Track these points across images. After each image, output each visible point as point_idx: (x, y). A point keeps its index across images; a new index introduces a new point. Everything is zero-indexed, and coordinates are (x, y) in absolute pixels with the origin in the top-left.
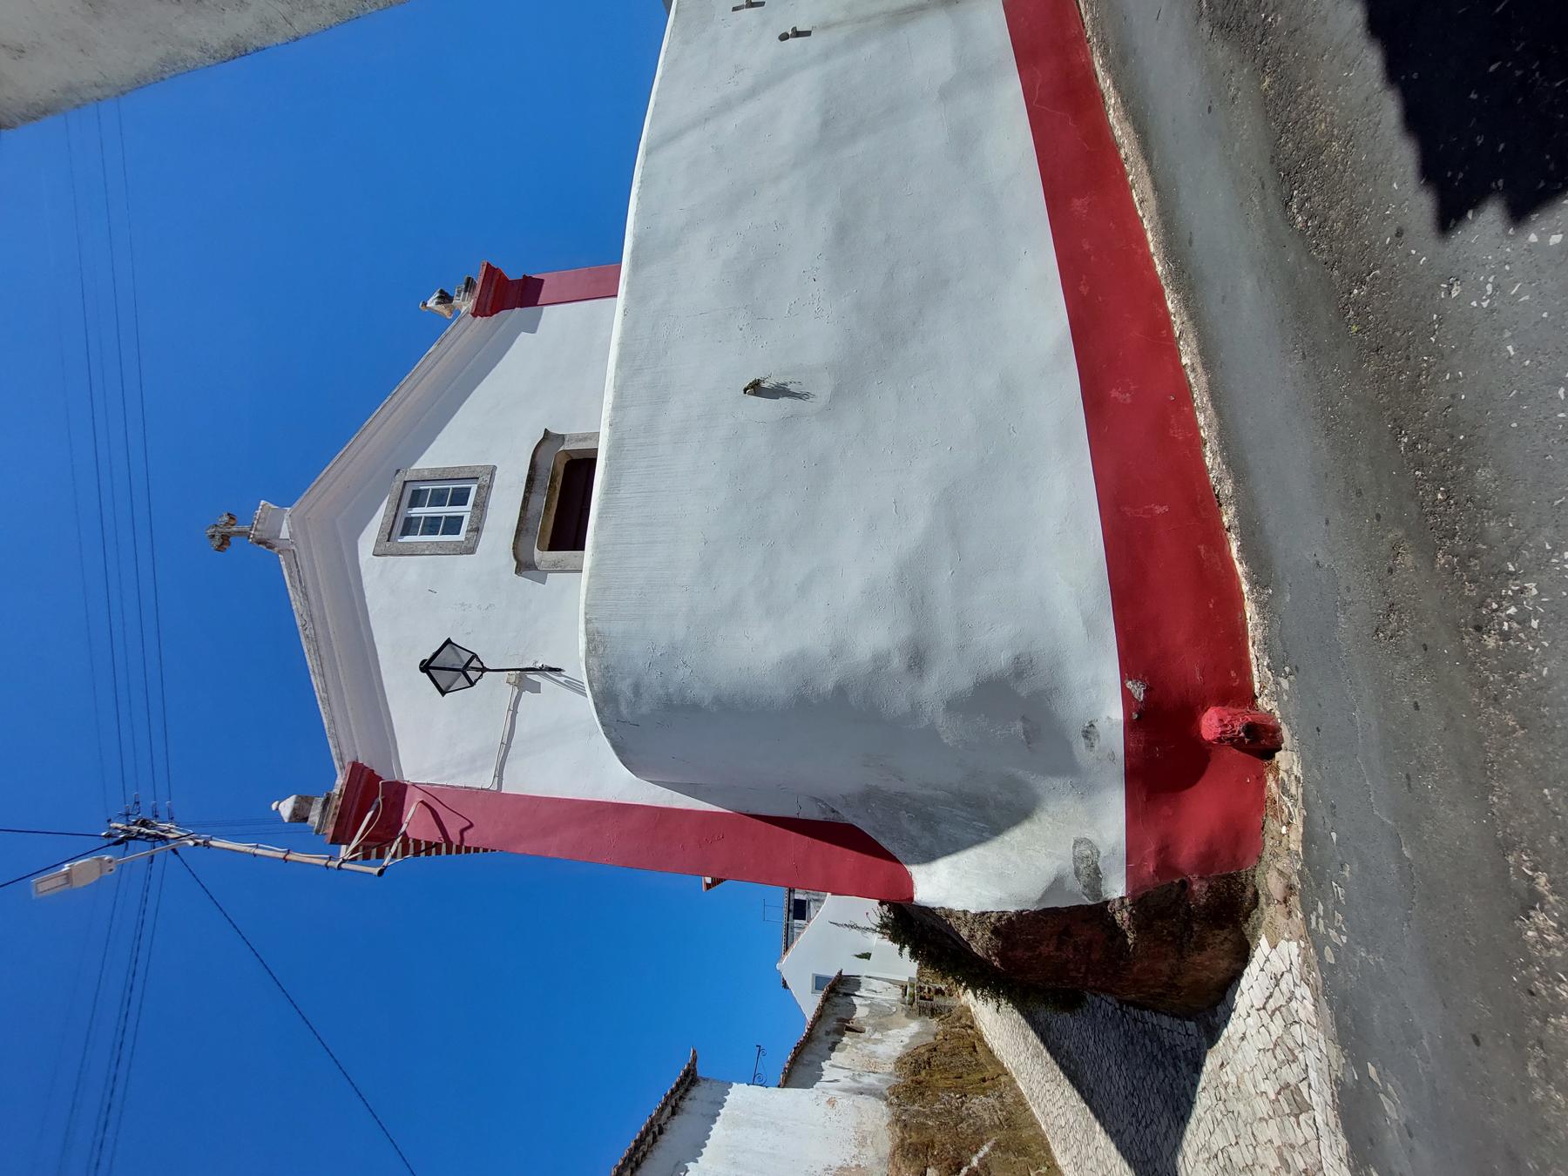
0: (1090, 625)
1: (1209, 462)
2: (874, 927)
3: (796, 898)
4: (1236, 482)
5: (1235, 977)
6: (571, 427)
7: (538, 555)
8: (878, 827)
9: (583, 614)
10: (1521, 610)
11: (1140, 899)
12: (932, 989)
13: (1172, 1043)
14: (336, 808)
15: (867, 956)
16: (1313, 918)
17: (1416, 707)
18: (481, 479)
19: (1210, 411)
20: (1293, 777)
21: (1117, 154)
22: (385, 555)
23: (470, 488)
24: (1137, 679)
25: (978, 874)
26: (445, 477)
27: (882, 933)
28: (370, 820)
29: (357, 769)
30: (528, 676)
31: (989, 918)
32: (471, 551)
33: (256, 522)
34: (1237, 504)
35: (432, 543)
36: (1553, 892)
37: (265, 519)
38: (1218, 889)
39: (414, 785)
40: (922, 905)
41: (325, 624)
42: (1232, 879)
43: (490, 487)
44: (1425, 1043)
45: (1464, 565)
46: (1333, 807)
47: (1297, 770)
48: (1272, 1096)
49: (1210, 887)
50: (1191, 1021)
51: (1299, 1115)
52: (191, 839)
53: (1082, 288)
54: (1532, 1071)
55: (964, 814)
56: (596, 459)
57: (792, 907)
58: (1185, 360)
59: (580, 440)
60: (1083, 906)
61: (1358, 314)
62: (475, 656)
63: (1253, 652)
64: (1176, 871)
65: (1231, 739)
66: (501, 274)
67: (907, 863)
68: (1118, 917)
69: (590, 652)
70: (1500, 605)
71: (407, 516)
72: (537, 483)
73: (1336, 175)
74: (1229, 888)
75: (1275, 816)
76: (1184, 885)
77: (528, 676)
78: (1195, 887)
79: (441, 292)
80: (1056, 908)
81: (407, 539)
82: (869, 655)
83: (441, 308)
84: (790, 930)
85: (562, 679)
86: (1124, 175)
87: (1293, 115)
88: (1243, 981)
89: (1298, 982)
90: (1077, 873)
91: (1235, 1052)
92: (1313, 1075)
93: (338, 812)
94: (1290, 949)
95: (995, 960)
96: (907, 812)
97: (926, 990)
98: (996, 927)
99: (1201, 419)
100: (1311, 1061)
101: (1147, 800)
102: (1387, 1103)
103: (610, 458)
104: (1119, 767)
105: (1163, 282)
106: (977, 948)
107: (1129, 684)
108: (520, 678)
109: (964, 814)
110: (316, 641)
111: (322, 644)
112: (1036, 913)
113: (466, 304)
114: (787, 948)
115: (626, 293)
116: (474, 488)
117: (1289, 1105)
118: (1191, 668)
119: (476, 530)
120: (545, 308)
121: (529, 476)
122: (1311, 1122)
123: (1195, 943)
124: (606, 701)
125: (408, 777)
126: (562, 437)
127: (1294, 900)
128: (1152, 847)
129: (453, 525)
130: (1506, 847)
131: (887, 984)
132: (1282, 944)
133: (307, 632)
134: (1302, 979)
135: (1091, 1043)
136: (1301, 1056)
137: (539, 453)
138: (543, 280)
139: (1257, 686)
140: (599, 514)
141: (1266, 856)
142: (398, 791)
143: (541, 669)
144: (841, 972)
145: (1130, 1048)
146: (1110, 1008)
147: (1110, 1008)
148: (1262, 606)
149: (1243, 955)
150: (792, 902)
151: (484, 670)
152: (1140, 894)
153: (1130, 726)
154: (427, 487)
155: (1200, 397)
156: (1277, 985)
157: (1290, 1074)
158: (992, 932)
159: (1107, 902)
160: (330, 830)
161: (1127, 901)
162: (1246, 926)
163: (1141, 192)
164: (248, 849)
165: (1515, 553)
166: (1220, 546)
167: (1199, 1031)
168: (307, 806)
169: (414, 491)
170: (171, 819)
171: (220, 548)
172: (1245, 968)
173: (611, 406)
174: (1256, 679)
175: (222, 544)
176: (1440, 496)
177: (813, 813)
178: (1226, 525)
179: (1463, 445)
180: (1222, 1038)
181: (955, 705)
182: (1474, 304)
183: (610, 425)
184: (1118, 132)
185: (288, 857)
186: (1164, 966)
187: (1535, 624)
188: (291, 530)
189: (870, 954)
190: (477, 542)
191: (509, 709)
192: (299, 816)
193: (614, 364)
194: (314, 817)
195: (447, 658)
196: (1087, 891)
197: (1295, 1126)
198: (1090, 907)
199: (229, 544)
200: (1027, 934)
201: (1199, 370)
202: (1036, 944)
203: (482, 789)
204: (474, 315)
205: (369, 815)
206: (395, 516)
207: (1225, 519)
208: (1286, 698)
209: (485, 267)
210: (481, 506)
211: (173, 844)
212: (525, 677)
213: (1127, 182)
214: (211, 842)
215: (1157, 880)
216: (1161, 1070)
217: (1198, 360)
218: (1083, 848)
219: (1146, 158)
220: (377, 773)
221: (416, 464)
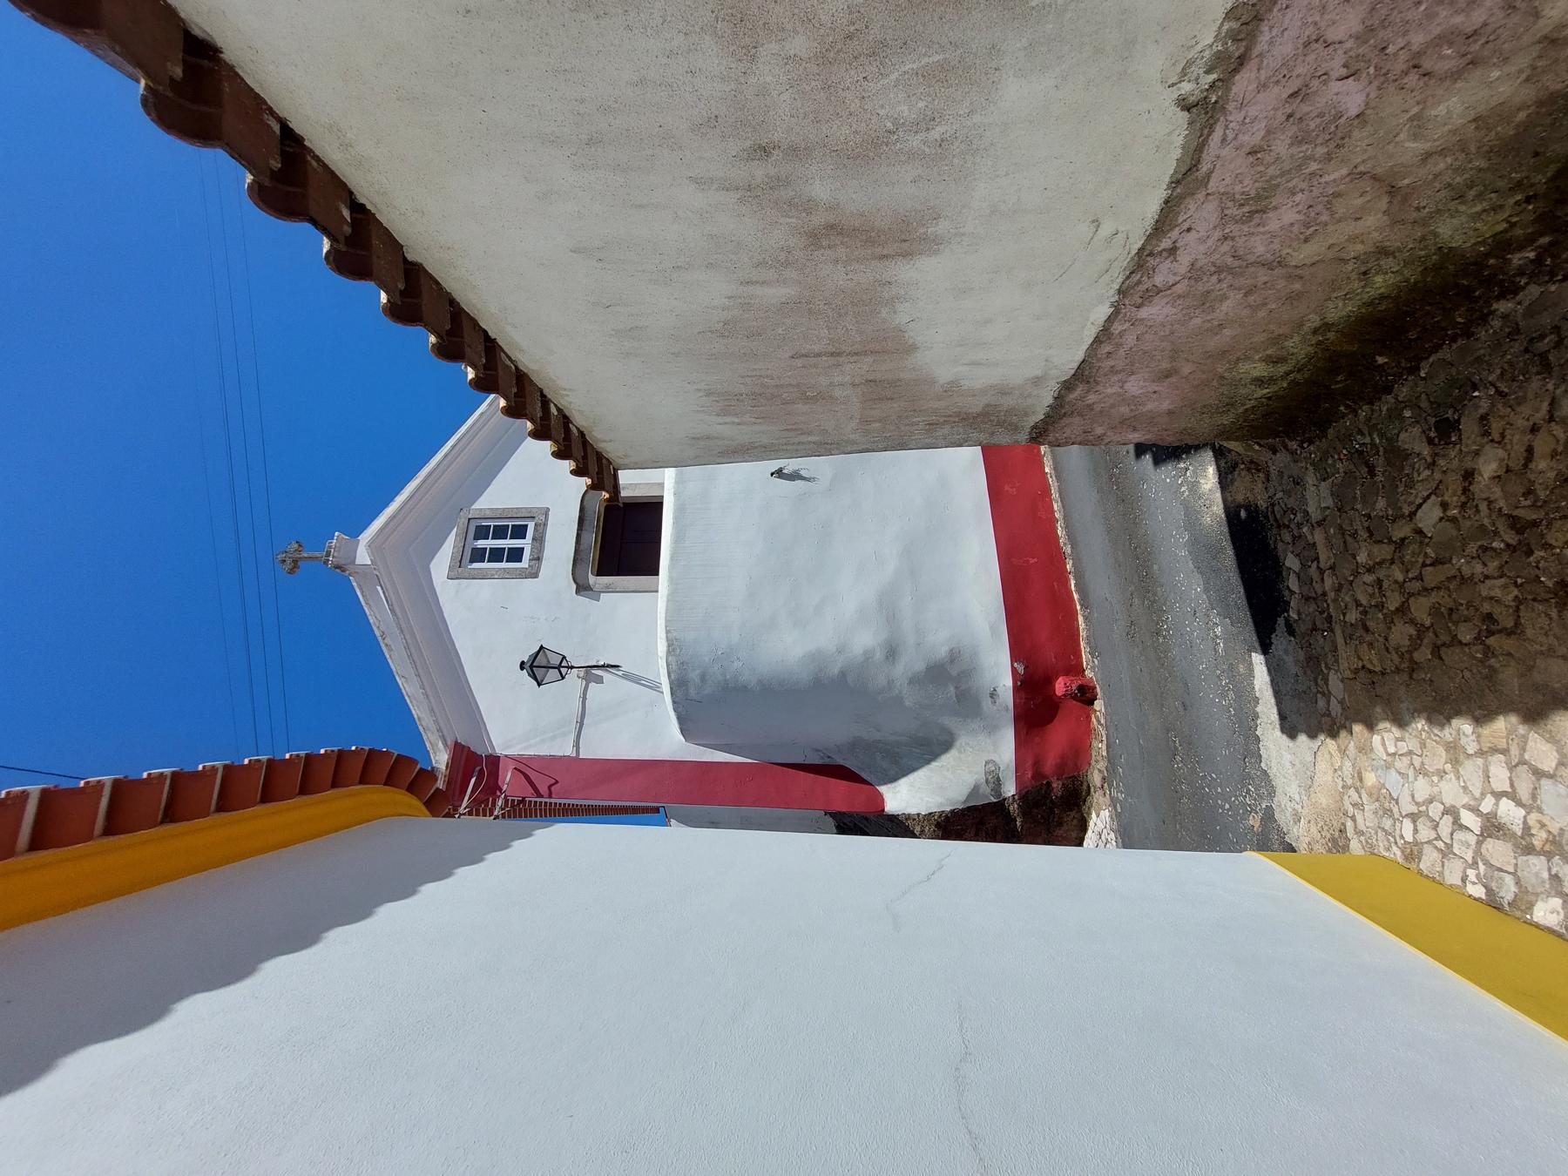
0: (993, 629)
1: (1059, 532)
4: (1072, 548)
18: (537, 518)
19: (1060, 504)
22: (457, 578)
23: (527, 526)
24: (1020, 662)
32: (535, 575)
37: (340, 547)
39: (506, 756)
40: (890, 813)
41: (413, 635)
42: (1074, 778)
43: (545, 525)
45: (1152, 605)
49: (1063, 784)
55: (918, 751)
58: (1047, 470)
62: (564, 657)
63: (1082, 644)
64: (1043, 776)
65: (1071, 694)
67: (880, 785)
68: (1011, 808)
72: (586, 523)
74: (1074, 785)
75: (1096, 738)
76: (1049, 784)
78: (1055, 785)
82: (861, 652)
85: (620, 673)
94: (1105, 814)
101: (1027, 733)
104: (1011, 714)
107: (670, 658)
108: (587, 672)
109: (918, 751)
112: (963, 810)
118: (1049, 655)
119: (537, 559)
121: (580, 517)
124: (679, 686)
125: (500, 749)
128: (1030, 763)
129: (516, 555)
130: (1168, 731)
133: (386, 641)
137: (586, 499)
139: (1085, 663)
141: (1093, 763)
142: (494, 761)
143: (603, 666)
148: (1086, 618)
152: (1024, 792)
153: (1016, 689)
155: (1055, 494)
158: (936, 826)
159: (1005, 799)
161: (1016, 797)
166: (1067, 581)
171: (291, 572)
174: (1084, 660)
175: (294, 567)
177: (815, 759)
181: (914, 681)
190: (539, 569)
195: (540, 660)
196: (993, 793)
198: (995, 803)
199: (298, 568)
205: (473, 780)
207: (1068, 567)
210: (539, 540)
212: (591, 673)
215: (1033, 783)
220: (472, 749)
221: (476, 504)
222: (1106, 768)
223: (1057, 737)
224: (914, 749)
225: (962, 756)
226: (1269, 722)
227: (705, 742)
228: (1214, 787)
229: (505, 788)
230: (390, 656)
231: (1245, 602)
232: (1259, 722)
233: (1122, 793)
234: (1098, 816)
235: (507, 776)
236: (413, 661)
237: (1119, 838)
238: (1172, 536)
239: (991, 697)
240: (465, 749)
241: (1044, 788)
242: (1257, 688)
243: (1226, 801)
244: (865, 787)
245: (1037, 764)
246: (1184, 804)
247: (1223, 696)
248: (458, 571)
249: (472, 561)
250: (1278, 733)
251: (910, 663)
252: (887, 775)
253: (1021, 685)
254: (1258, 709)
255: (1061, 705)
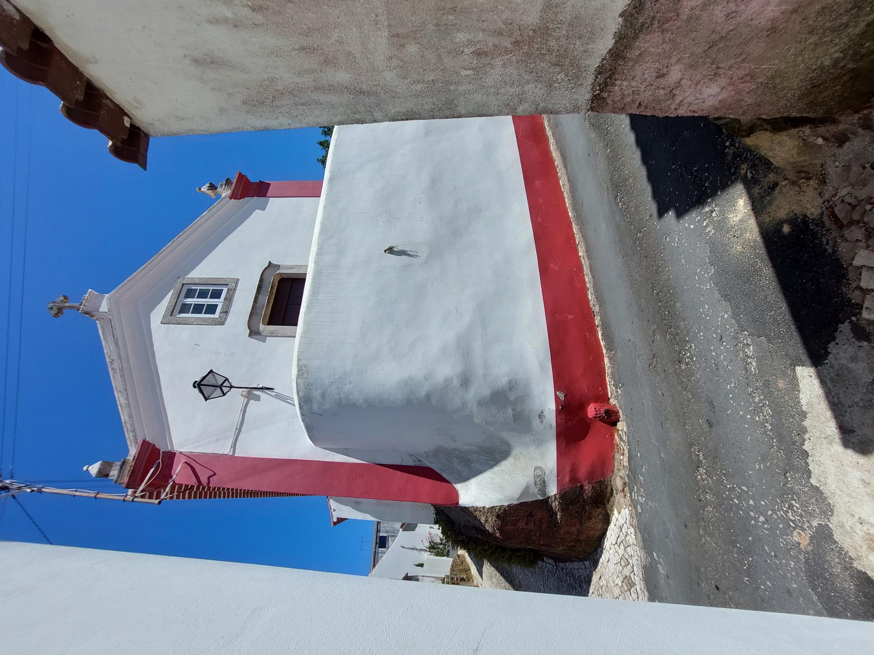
0: (541, 366)
1: (590, 297)
2: (426, 549)
3: (381, 535)
5: (605, 531)
6: (288, 263)
7: (262, 327)
8: (442, 467)
9: (296, 356)
10: (691, 354)
11: (563, 495)
12: (459, 578)
13: (579, 575)
14: (131, 466)
15: (421, 565)
16: (633, 494)
17: (663, 395)
18: (229, 285)
20: (624, 433)
21: (554, 164)
22: (168, 324)
23: (222, 290)
25: (490, 487)
26: (208, 283)
27: (430, 552)
28: (151, 475)
29: (145, 444)
30: (254, 392)
31: (495, 509)
32: (223, 323)
33: (84, 301)
34: (601, 315)
35: (199, 318)
36: (704, 459)
37: (90, 300)
38: (596, 489)
39: (181, 453)
40: (463, 506)
41: (128, 361)
42: (601, 483)
43: (235, 290)
44: (671, 534)
46: (638, 442)
47: (625, 429)
48: (620, 585)
50: (586, 561)
51: (630, 589)
52: (29, 488)
53: (539, 219)
54: (701, 532)
55: (484, 458)
56: (305, 279)
57: (378, 541)
58: (580, 254)
59: (289, 268)
60: (538, 500)
61: (639, 243)
62: (227, 379)
63: (608, 379)
64: (578, 481)
65: (600, 417)
66: (247, 178)
67: (456, 483)
68: (553, 505)
69: (300, 375)
70: (685, 353)
71: (184, 303)
72: (263, 289)
73: (632, 191)
74: (601, 488)
75: (618, 452)
76: (582, 487)
77: (254, 392)
79: (211, 184)
80: (526, 503)
81: (183, 315)
82: (443, 379)
83: (210, 192)
84: (376, 554)
85: (273, 394)
86: (556, 173)
87: (617, 165)
88: (608, 533)
89: (629, 527)
90: (535, 483)
91: (605, 569)
92: (635, 568)
93: (132, 469)
94: (626, 512)
95: (497, 533)
96: (457, 459)
97: (455, 579)
98: (498, 514)
99: (587, 279)
100: (635, 564)
101: (566, 447)
102: (661, 568)
103: (314, 279)
104: (554, 432)
105: (572, 220)
106: (488, 527)
108: (249, 393)
109: (484, 458)
110: (122, 370)
111: (126, 372)
112: (517, 505)
113: (225, 192)
114: (374, 566)
115: (326, 199)
116: (225, 290)
117: (627, 586)
118: (584, 386)
119: (226, 312)
120: (271, 199)
121: (259, 285)
122: (635, 591)
123: (587, 516)
124: (305, 401)
125: (177, 448)
126: (278, 267)
127: (626, 489)
128: (568, 470)
129: (212, 309)
130: (691, 445)
131: (433, 579)
132: (623, 510)
134: (630, 525)
135: (542, 587)
136: (631, 561)
137: (265, 273)
138: (270, 184)
139: (609, 394)
140: (308, 306)
141: (616, 471)
142: (170, 456)
143: (261, 388)
144: (407, 574)
145: (560, 584)
146: (551, 566)
147: (551, 566)
148: (610, 359)
149: (607, 521)
150: (378, 538)
151: (231, 387)
153: (559, 412)
154: (197, 288)
155: (586, 270)
156: (621, 531)
157: (627, 571)
159: (549, 498)
160: (126, 479)
161: (557, 496)
162: (608, 505)
163: (563, 182)
164: (70, 493)
165: (688, 334)
167: (590, 564)
168: (108, 467)
169: (188, 289)
170: (12, 477)
171: (56, 315)
172: (608, 526)
173: (315, 253)
174: (609, 391)
175: (58, 313)
176: (666, 313)
177: (409, 462)
178: (597, 324)
179: (672, 294)
180: (600, 564)
181: (483, 403)
182: (673, 244)
183: (315, 262)
184: (554, 155)
185: (98, 496)
186: (574, 530)
187: (694, 359)
188: (109, 307)
189: (423, 564)
190: (226, 319)
191: (241, 410)
192: (103, 474)
193: (318, 233)
194: (114, 473)
195: (210, 380)
196: (540, 493)
197: (629, 595)
198: (541, 500)
200: (513, 517)
201: (586, 258)
202: (517, 522)
203: (223, 454)
204: (230, 198)
206: (176, 303)
207: (596, 322)
208: (620, 398)
209: (238, 174)
210: (229, 300)
211: (12, 492)
212: (252, 392)
213: (557, 176)
214: (43, 490)
216: (574, 590)
217: (585, 254)
218: (538, 471)
219: (565, 168)
220: (157, 447)
222: (628, 475)
223: (588, 449)
224: (482, 457)
225: (517, 462)
226: (823, 436)
227: (330, 447)
228: (745, 500)
229: (174, 477)
230: (114, 377)
231: (788, 317)
232: (806, 436)
233: (642, 496)
234: (619, 513)
235: (178, 469)
236: (124, 379)
237: (638, 532)
238: (696, 274)
239: (540, 418)
240: (150, 446)
241: (578, 489)
242: (803, 402)
243: (761, 514)
244: (445, 484)
245: (573, 471)
246: (708, 511)
247: (758, 410)
248: (170, 318)
249: (180, 312)
250: (838, 448)
251: (479, 389)
252: (461, 476)
253: (562, 409)
254: (806, 423)
255: (591, 425)
